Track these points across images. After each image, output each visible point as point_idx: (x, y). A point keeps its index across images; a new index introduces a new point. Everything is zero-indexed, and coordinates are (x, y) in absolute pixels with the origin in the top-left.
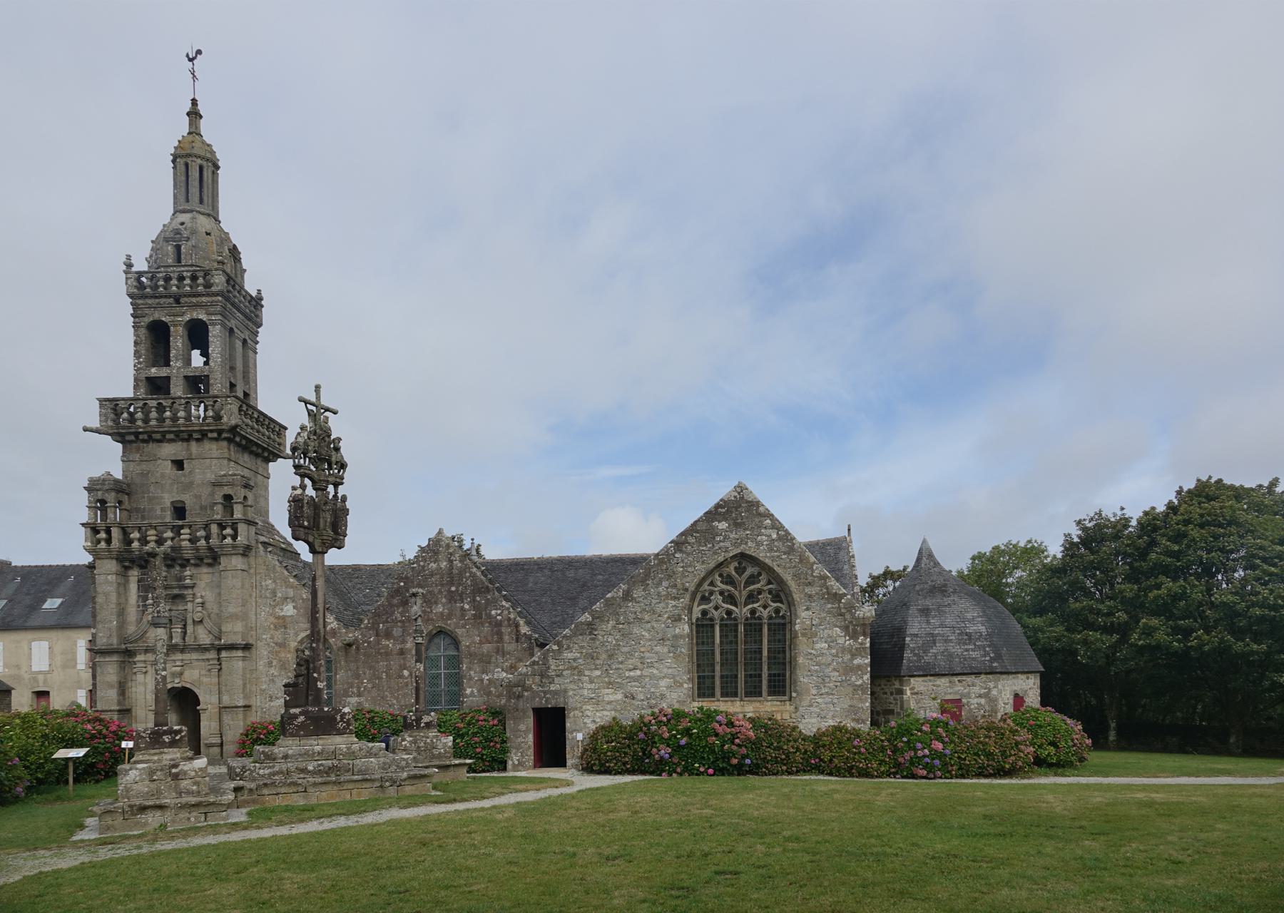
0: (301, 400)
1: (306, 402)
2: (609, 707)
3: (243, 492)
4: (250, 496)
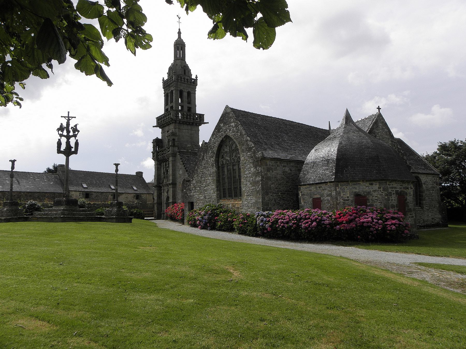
0: (62, 117)
1: (65, 117)
2: (201, 202)
3: (172, 137)
4: (176, 138)
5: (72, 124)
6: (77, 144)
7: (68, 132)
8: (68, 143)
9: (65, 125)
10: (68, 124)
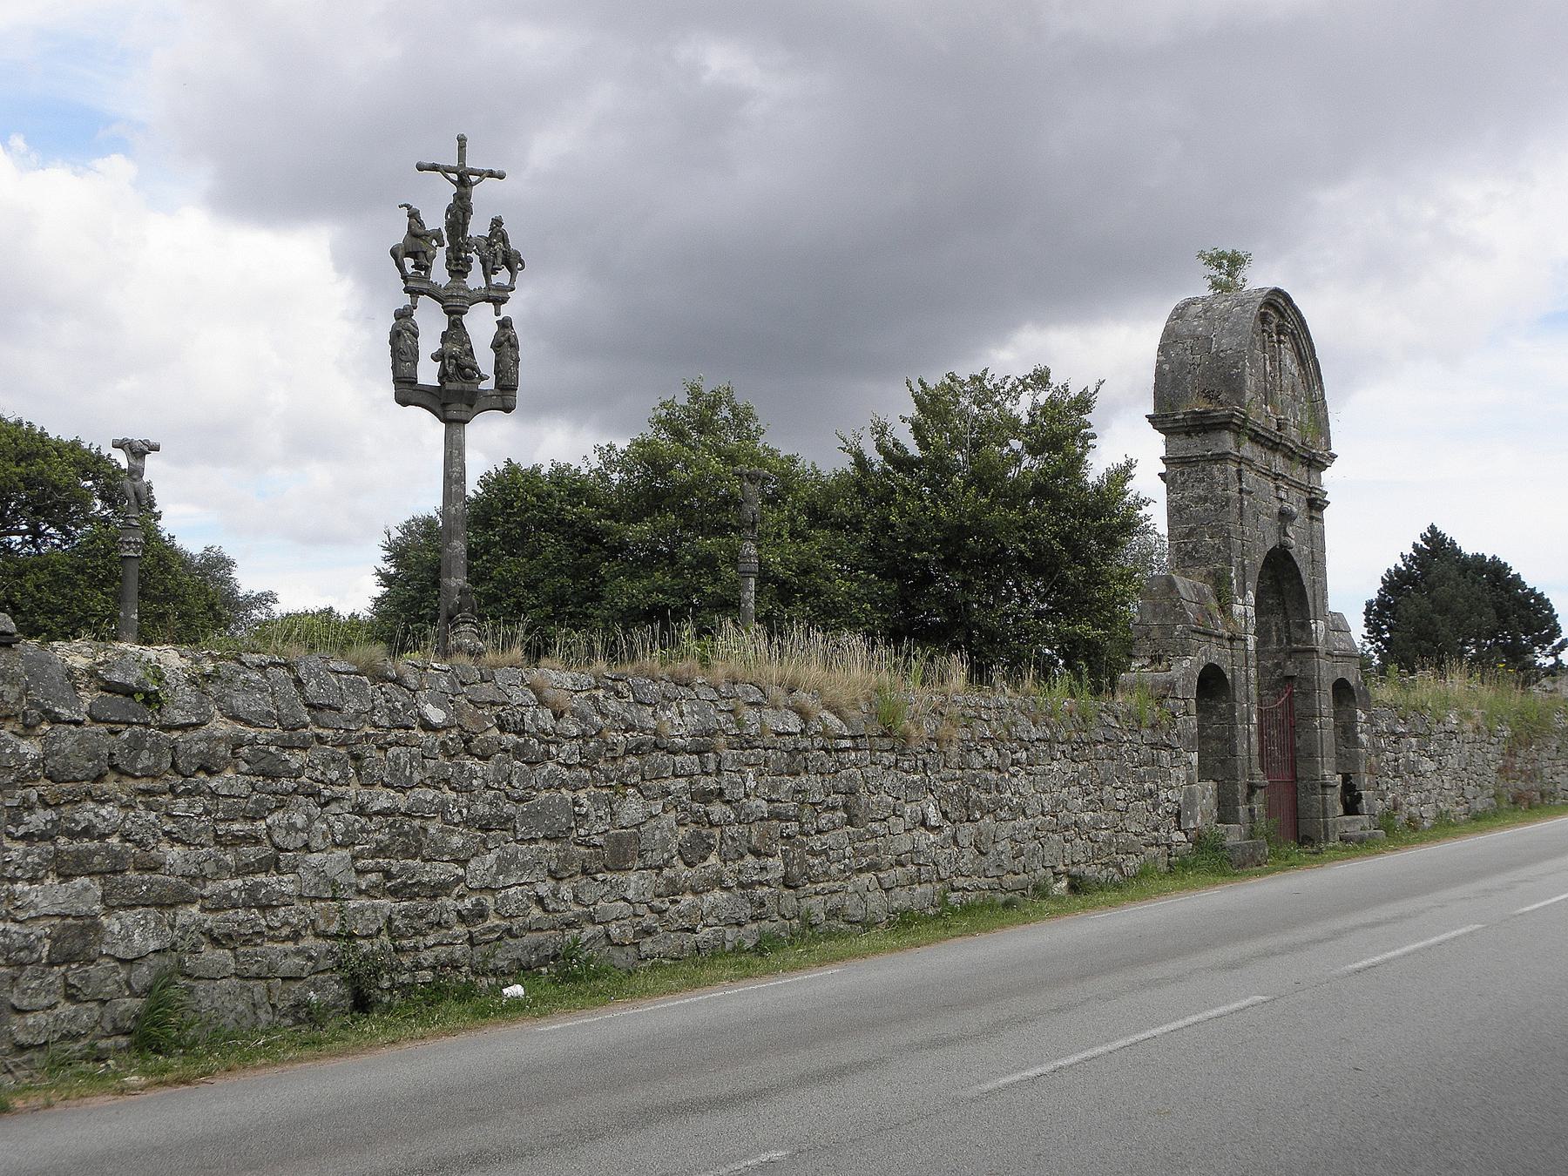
5: (478, 227)
6: (505, 342)
7: (458, 268)
8: (455, 332)
9: (435, 220)
10: (460, 212)
